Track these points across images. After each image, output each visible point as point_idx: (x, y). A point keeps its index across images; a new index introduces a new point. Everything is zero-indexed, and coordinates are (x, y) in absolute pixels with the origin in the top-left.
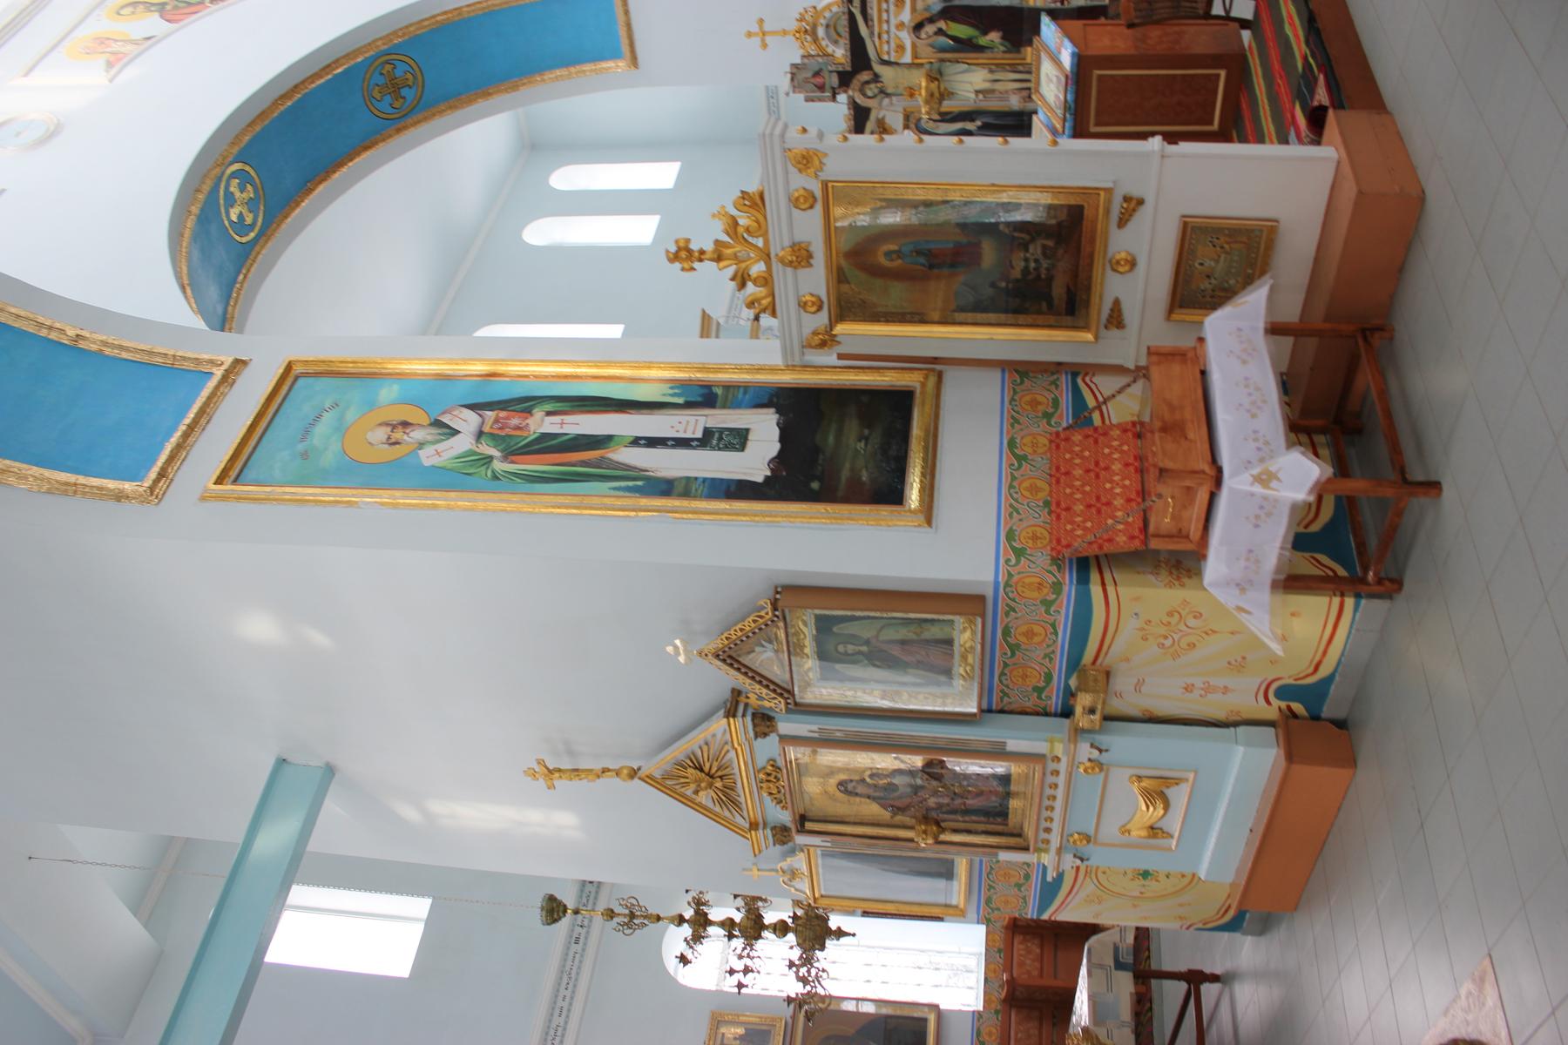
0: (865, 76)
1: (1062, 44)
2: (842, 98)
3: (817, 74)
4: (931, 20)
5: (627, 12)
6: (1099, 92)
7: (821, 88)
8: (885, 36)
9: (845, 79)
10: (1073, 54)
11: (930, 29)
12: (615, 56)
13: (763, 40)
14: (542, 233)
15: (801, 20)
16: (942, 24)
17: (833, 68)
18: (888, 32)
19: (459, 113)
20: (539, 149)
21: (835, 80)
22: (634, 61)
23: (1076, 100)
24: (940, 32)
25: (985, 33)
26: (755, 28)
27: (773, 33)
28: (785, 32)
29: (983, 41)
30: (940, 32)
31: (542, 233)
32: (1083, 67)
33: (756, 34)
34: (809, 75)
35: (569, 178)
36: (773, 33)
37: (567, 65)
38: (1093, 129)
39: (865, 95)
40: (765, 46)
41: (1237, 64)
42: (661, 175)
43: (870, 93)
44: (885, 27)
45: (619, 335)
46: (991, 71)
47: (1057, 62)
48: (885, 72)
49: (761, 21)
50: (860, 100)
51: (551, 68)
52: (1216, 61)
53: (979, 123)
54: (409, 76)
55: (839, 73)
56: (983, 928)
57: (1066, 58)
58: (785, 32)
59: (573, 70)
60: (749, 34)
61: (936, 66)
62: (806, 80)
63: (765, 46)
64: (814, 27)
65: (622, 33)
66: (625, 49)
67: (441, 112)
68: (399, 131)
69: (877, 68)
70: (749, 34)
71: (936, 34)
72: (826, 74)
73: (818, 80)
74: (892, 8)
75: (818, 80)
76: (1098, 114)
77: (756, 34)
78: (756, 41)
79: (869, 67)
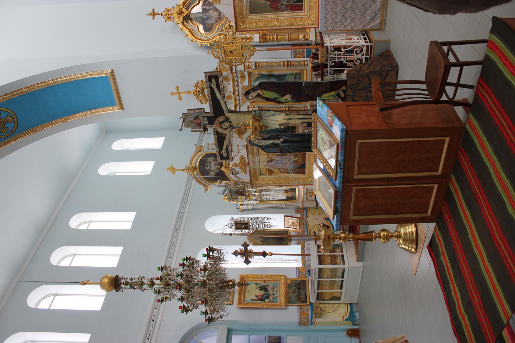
0: (221, 119)
1: (333, 120)
2: (211, 130)
3: (196, 118)
4: (254, 90)
5: (116, 85)
6: (360, 154)
7: (199, 125)
8: (237, 93)
9: (211, 121)
10: (342, 131)
11: (254, 94)
12: (113, 104)
13: (179, 96)
14: (106, 170)
15: (196, 86)
16: (260, 92)
17: (205, 115)
18: (238, 91)
19: (39, 133)
20: (109, 133)
21: (206, 121)
22: (122, 107)
23: (344, 160)
24: (259, 95)
25: (283, 96)
26: (175, 91)
27: (184, 93)
28: (189, 92)
29: (282, 99)
30: (259, 95)
31: (106, 170)
32: (349, 136)
33: (176, 93)
34: (193, 119)
35: (119, 145)
36: (184, 93)
37: (91, 109)
38: (356, 177)
39: (222, 128)
40: (180, 99)
41: (460, 135)
42: (156, 143)
43: (224, 127)
44: (237, 88)
45: (128, 226)
46: (287, 115)
47: (330, 133)
48: (232, 117)
49: (178, 87)
50: (219, 130)
51: (78, 112)
52: (443, 132)
53: (282, 140)
54: (9, 117)
55: (207, 117)
56: (300, 245)
57: (337, 129)
58: (189, 92)
59: (93, 111)
60: (173, 94)
61: (258, 112)
62: (191, 121)
63: (180, 99)
64: (203, 90)
65: (115, 94)
66: (117, 101)
67: (28, 133)
68: (5, 144)
69: (227, 114)
70: (173, 94)
71: (256, 96)
72: (201, 118)
73: (197, 121)
74: (239, 80)
75: (197, 121)
76: (359, 167)
77: (176, 93)
78: (176, 96)
79: (223, 114)
